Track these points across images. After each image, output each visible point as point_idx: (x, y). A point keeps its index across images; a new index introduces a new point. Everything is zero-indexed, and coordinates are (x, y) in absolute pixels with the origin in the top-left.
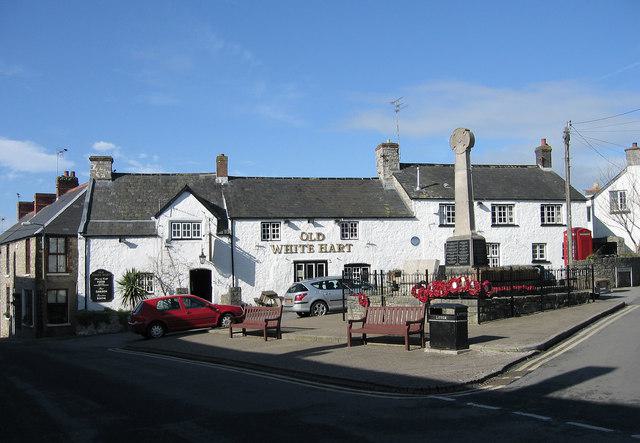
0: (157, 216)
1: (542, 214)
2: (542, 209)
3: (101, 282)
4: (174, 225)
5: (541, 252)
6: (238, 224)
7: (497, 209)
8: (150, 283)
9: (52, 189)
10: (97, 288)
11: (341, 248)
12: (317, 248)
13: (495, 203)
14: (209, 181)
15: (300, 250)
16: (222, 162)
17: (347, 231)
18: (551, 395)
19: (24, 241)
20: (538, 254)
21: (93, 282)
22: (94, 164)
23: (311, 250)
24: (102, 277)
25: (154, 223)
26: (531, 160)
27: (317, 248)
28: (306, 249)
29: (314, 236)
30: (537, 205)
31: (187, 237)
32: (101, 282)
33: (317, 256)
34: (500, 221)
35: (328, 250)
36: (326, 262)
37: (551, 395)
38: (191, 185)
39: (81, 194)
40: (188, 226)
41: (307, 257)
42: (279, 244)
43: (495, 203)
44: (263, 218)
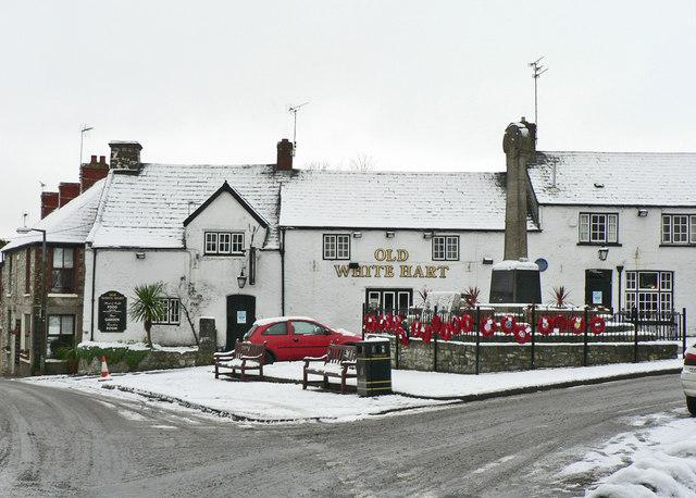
3: (112, 308)
4: (210, 236)
12: (397, 270)
15: (373, 272)
21: (102, 307)
23: (389, 271)
27: (397, 270)
28: (383, 272)
29: (395, 254)
32: (112, 308)
33: (397, 282)
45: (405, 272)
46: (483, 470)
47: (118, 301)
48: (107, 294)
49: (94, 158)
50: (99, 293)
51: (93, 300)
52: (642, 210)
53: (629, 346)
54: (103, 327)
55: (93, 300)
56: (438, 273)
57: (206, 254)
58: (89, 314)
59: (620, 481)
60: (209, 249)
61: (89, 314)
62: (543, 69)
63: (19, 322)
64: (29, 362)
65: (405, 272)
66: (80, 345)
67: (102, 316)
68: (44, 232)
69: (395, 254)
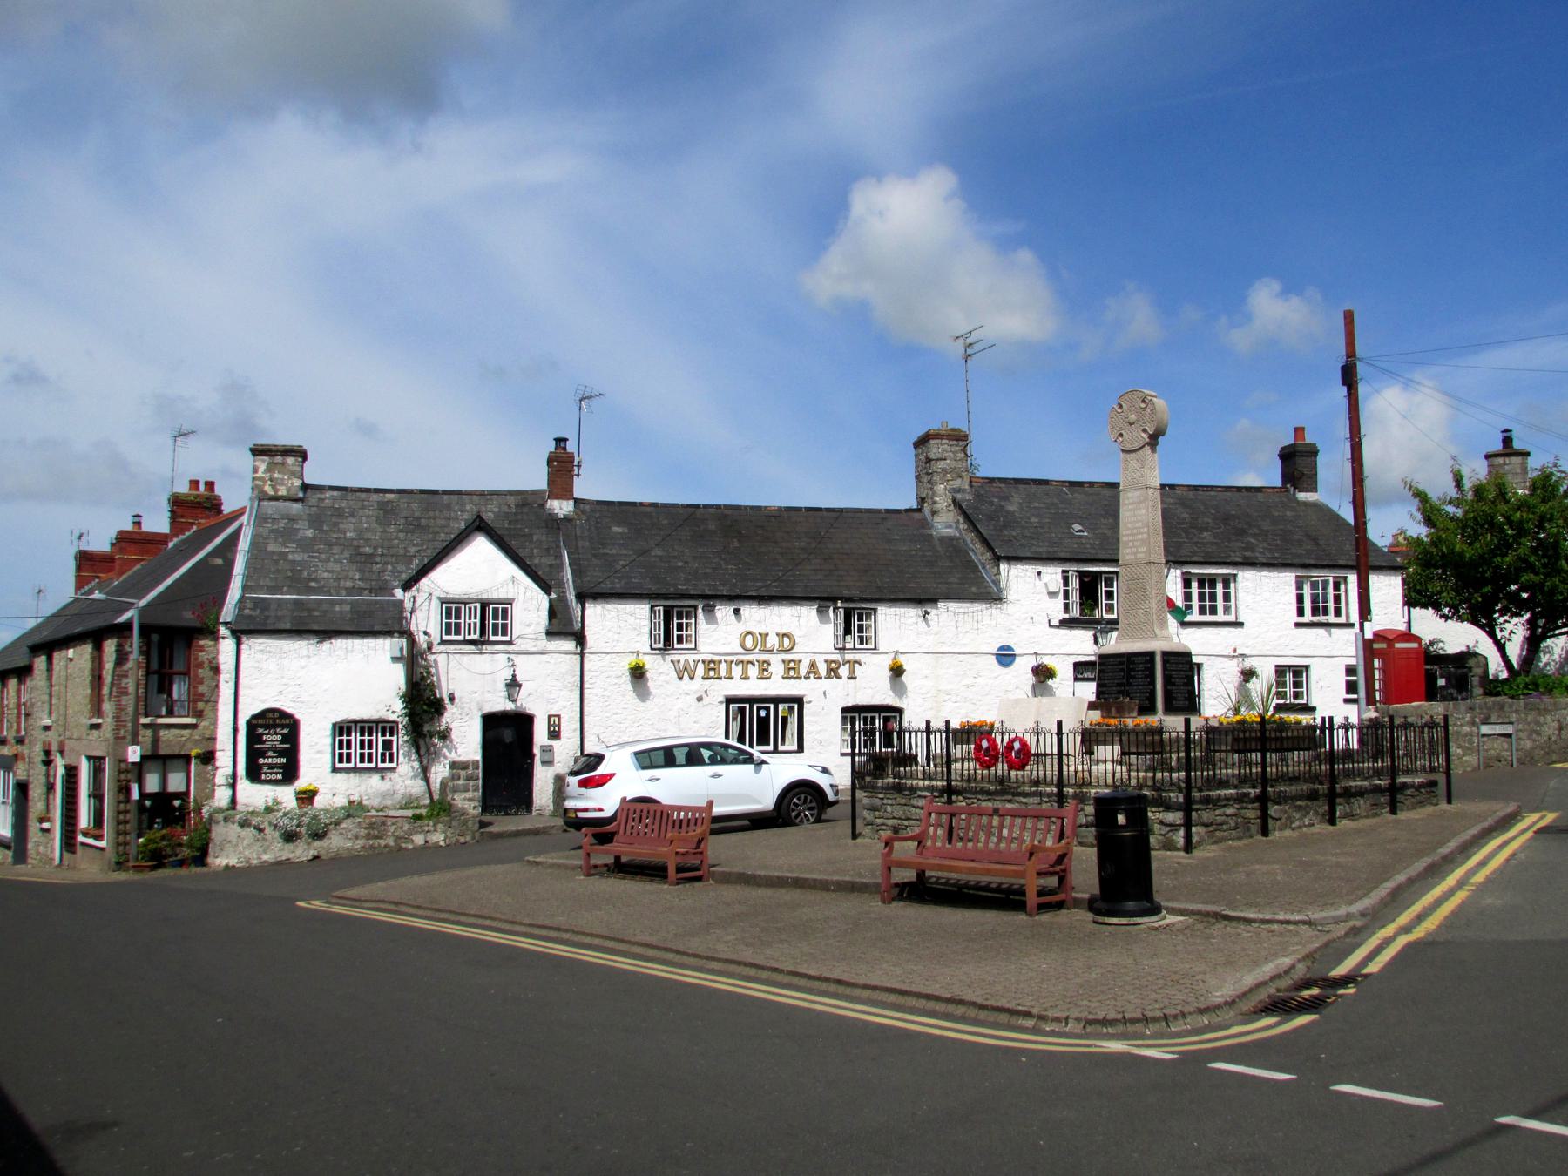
0: (407, 587)
1: (1300, 599)
2: (1299, 587)
3: (273, 739)
4: (451, 608)
5: (1297, 685)
6: (255, 648)
7: (1195, 585)
8: (387, 745)
9: (158, 522)
10: (263, 753)
11: (833, 672)
12: (777, 669)
13: (852, 605)
14: (528, 502)
15: (737, 671)
16: (562, 466)
17: (854, 623)
18: (1209, 1065)
19: (87, 649)
20: (1289, 690)
21: (253, 737)
22: (263, 464)
23: (764, 666)
24: (275, 726)
25: (401, 602)
26: (1267, 474)
27: (777, 669)
28: (753, 671)
29: (772, 641)
30: (1287, 579)
31: (453, 637)
32: (273, 739)
33: (777, 686)
34: (1202, 611)
35: (803, 672)
36: (799, 701)
37: (1209, 1065)
38: (488, 516)
39: (229, 531)
40: (458, 610)
41: (754, 687)
42: (691, 657)
43: (852, 605)
44: (666, 597)
45: (791, 670)
46: (1318, 857)
47: (283, 726)
48: (263, 714)
49: (194, 484)
50: (248, 710)
51: (236, 730)
52: (966, 351)
53: (1419, 1108)
54: (254, 774)
55: (236, 730)
56: (844, 671)
57: (443, 642)
58: (229, 753)
59: (1480, 817)
60: (448, 632)
61: (229, 753)
62: (977, 347)
63: (72, 773)
64: (103, 844)
65: (791, 670)
66: (1527, 616)
67: (253, 755)
68: (1050, 626)
69: (772, 641)
